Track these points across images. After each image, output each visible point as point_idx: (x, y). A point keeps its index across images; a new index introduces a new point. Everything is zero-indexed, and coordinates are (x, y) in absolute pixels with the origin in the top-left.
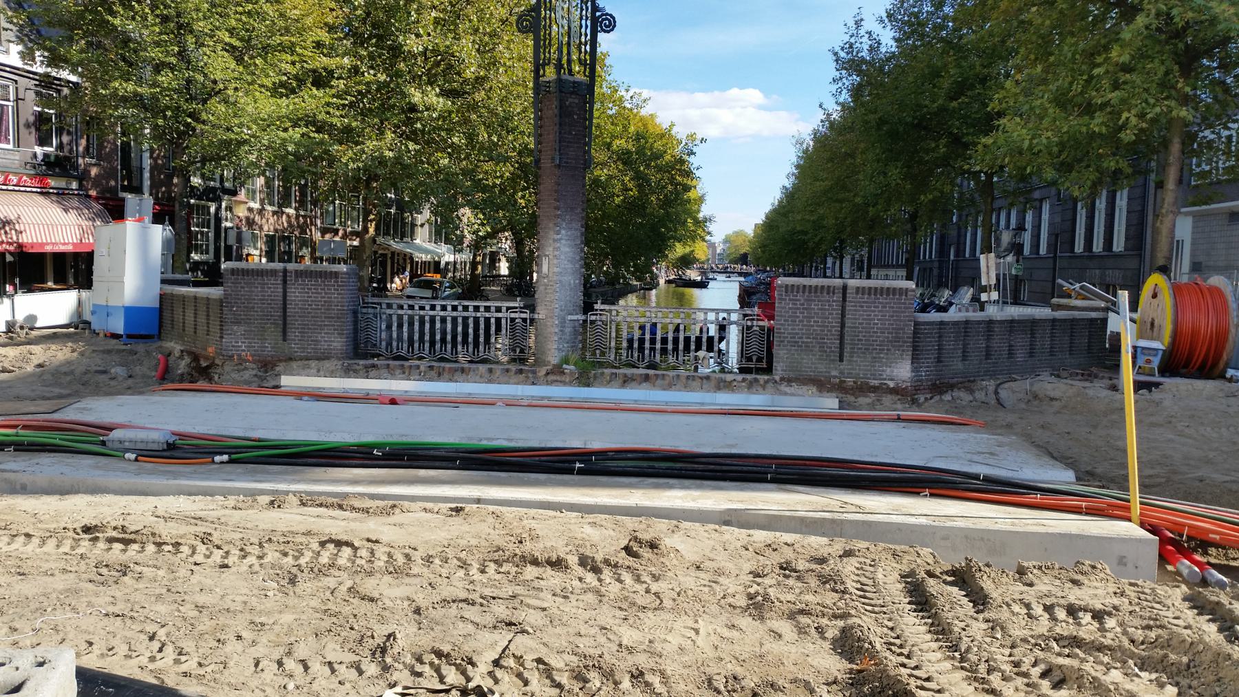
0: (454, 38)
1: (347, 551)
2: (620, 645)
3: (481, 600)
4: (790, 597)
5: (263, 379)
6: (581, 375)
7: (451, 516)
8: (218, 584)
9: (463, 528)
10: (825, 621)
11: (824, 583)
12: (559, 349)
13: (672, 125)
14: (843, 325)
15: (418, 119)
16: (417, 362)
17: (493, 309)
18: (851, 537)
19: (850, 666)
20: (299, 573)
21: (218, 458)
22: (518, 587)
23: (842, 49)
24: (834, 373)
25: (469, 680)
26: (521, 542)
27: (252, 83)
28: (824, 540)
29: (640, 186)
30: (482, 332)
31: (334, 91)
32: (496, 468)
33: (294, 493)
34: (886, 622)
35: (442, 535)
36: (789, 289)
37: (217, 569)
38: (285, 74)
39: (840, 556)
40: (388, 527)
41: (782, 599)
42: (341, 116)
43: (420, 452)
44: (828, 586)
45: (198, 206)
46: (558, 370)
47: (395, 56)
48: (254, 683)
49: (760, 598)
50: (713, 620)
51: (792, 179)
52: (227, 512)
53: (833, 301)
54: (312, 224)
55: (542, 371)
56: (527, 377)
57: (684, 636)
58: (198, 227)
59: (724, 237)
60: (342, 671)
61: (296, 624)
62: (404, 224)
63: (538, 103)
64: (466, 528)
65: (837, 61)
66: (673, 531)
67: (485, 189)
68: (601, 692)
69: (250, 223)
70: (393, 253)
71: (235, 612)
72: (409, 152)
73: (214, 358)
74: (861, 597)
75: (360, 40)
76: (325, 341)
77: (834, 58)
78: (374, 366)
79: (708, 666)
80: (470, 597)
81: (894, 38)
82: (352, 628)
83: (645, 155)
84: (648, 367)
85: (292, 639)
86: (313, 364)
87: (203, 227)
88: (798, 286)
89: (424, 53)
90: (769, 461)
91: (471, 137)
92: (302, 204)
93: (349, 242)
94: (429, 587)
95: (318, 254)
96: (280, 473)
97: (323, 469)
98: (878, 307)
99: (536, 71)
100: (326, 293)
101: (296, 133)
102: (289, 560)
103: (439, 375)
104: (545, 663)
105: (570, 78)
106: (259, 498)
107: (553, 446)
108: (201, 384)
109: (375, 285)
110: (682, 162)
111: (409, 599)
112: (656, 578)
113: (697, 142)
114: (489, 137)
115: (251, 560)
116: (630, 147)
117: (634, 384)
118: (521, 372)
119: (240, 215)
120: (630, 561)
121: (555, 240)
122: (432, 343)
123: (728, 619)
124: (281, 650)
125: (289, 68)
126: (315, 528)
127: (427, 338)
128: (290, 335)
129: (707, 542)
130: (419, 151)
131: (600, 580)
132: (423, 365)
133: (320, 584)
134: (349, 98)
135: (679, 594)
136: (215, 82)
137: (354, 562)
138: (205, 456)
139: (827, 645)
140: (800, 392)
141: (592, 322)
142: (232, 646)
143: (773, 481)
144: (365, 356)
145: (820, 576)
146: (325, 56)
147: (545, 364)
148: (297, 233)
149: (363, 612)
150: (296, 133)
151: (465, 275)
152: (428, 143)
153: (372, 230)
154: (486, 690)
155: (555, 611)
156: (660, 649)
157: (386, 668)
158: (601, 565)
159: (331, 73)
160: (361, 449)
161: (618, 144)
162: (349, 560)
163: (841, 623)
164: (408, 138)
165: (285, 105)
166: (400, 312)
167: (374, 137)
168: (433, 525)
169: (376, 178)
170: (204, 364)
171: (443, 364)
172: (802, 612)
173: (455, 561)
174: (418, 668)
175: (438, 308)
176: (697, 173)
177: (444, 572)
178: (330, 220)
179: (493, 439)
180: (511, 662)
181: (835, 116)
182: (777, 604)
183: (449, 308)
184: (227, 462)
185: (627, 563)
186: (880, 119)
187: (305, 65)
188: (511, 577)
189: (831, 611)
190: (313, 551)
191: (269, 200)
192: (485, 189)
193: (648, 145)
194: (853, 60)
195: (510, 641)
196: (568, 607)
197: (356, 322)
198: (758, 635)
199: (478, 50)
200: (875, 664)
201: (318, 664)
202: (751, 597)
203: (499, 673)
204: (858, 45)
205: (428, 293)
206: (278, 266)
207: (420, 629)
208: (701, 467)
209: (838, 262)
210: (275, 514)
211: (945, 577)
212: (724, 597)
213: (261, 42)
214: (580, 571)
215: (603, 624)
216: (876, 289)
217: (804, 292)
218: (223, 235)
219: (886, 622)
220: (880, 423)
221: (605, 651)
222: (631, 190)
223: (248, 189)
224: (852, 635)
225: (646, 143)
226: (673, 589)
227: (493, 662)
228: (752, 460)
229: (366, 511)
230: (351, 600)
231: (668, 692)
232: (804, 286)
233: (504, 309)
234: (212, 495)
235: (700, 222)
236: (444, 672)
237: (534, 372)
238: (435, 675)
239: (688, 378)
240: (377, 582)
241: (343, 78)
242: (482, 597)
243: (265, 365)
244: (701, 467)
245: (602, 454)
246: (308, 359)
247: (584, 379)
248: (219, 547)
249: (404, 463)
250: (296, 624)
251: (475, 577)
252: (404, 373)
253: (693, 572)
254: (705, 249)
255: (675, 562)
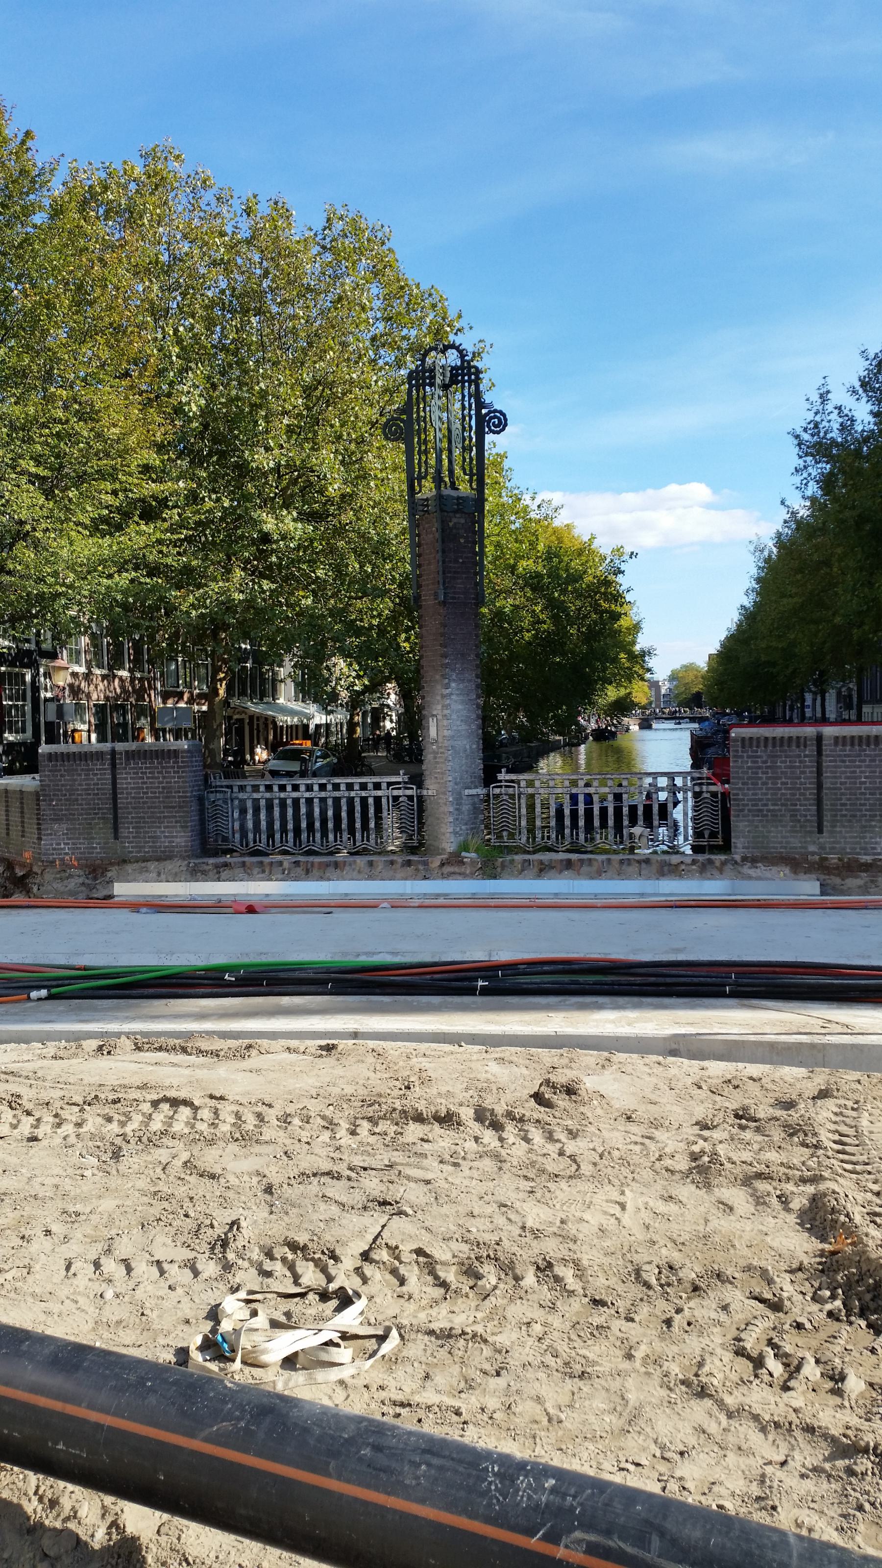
0: (312, 449)
1: (185, 1112)
2: (523, 1228)
3: (349, 1173)
4: (747, 1156)
5: (91, 888)
6: (485, 864)
7: (321, 1056)
8: (25, 1163)
9: (335, 1072)
10: (790, 1187)
11: (791, 1135)
12: (455, 833)
13: (593, 537)
14: (820, 786)
15: (273, 551)
16: (279, 858)
17: (370, 786)
18: (837, 1066)
19: (821, 1246)
20: (124, 1145)
21: (34, 994)
22: (396, 1153)
23: (805, 430)
24: (812, 848)
25: (330, 1279)
26: (408, 1088)
27: (68, 520)
28: (802, 1072)
29: (555, 618)
30: (358, 815)
31: (166, 525)
32: (378, 991)
33: (128, 1035)
34: (871, 1186)
35: (309, 1083)
36: (747, 743)
37: (25, 1143)
38: (107, 507)
39: (814, 1098)
40: (243, 1073)
41: (735, 1159)
42: (179, 554)
43: (282, 975)
44: (796, 1139)
45: (10, 674)
46: (455, 859)
47: (242, 476)
48: (64, 1292)
49: (706, 1159)
50: (645, 1190)
51: (752, 596)
52: (45, 1063)
53: (806, 756)
54: (150, 688)
55: (436, 862)
56: (417, 870)
57: (605, 1213)
58: (11, 699)
59: (669, 673)
60: (173, 1273)
61: (118, 1211)
62: (263, 681)
63: (414, 524)
64: (339, 1071)
65: (799, 445)
66: (603, 1067)
67: (358, 632)
68: (497, 1292)
69: (75, 691)
70: (251, 718)
71: (43, 1199)
72: (264, 592)
73: (31, 865)
74: (838, 1152)
75: (197, 460)
76: (165, 837)
77: (796, 442)
78: (226, 865)
79: (637, 1252)
80: (335, 1168)
81: (871, 412)
82: (186, 1216)
83: (559, 577)
84: (568, 851)
85: (114, 1232)
86: (152, 866)
87: (17, 700)
88: (758, 738)
89: (277, 469)
90: (727, 969)
91: (339, 571)
92: (137, 663)
93: (196, 708)
94: (284, 1158)
95: (157, 725)
96: (110, 1009)
97: (163, 1002)
98: (864, 761)
99: (411, 487)
100: (164, 778)
101: (123, 580)
102: (114, 1127)
103: (308, 872)
104: (426, 1255)
105: (453, 493)
106: (84, 1043)
107: (449, 959)
108: (18, 898)
109: (230, 759)
110: (607, 583)
111: (258, 1174)
112: (573, 1134)
113: (626, 557)
114: (361, 567)
115: (68, 1129)
116: (540, 569)
117: (553, 871)
118: (409, 863)
119: (61, 684)
120: (540, 1112)
121: (443, 696)
122: (297, 831)
123: (664, 1188)
124: (100, 1247)
125: (109, 499)
126: (152, 1079)
127: (290, 826)
128: (123, 832)
129: (647, 1079)
130: (275, 590)
131: (501, 1139)
132: (287, 860)
133: (149, 1158)
134: (185, 532)
135: (601, 1157)
136: (21, 523)
137: (193, 1127)
138: (19, 991)
139: (792, 1219)
140: (768, 875)
141: (497, 796)
142: (40, 1244)
143: (734, 995)
144: (215, 854)
145: (786, 1126)
146: (154, 481)
147: (438, 851)
148: (132, 700)
149: (201, 1194)
150: (123, 580)
151: (342, 739)
152: (286, 579)
153: (222, 692)
154: (350, 1292)
155: (443, 1184)
156: (574, 1232)
157: (227, 1267)
158: (503, 1120)
159: (163, 503)
160: (209, 974)
161: (524, 565)
162: (187, 1123)
163: (810, 1189)
164: (262, 576)
165: (106, 546)
166: (256, 796)
167: (219, 577)
168: (298, 1069)
169: (225, 627)
170: (20, 872)
171: (311, 859)
172: (759, 1176)
173: (319, 1120)
174: (268, 1266)
175: (302, 788)
176: (629, 597)
177: (305, 1135)
178: (172, 681)
179: (374, 954)
180: (383, 1255)
181: (803, 513)
182: (728, 1166)
183: (316, 788)
184: (46, 999)
185: (536, 1116)
186: (859, 516)
187: (130, 495)
188: (388, 1138)
189: (799, 1173)
190: (143, 1114)
191: (97, 660)
192: (358, 632)
193: (563, 564)
194: (819, 443)
195: (383, 1227)
196: (459, 1178)
197: (202, 811)
198: (702, 1209)
199: (342, 462)
200: (853, 1244)
201: (144, 1264)
202: (695, 1157)
203: (368, 1270)
204: (824, 424)
205: (295, 766)
206: (107, 746)
207: (271, 1213)
208: (638, 980)
209: (819, 698)
210: (104, 1063)
211: (571, 1282)
212: (660, 1159)
213: (74, 471)
214: (475, 1128)
215: (503, 1199)
216: (860, 737)
217: (766, 746)
218: (42, 708)
219: (871, 1186)
220: (876, 912)
221: (504, 1236)
222: (545, 622)
223: (71, 649)
224: (824, 1204)
225: (560, 562)
226: (594, 1150)
227: (362, 1255)
228: (705, 969)
229: (216, 1054)
230: (187, 1177)
231: (584, 1289)
232: (766, 739)
233: (384, 786)
234: (27, 1042)
235: (636, 657)
236: (299, 1270)
237: (426, 863)
238: (288, 1274)
239: (622, 862)
240: (220, 1152)
241: (179, 507)
242: (350, 1169)
243: (94, 871)
244: (638, 980)
245: (511, 967)
246: (145, 860)
247: (489, 870)
248: (29, 1113)
249: (262, 989)
250: (118, 1211)
251: (342, 1142)
252: (263, 872)
253: (622, 1124)
254: (646, 689)
255: (599, 1111)
